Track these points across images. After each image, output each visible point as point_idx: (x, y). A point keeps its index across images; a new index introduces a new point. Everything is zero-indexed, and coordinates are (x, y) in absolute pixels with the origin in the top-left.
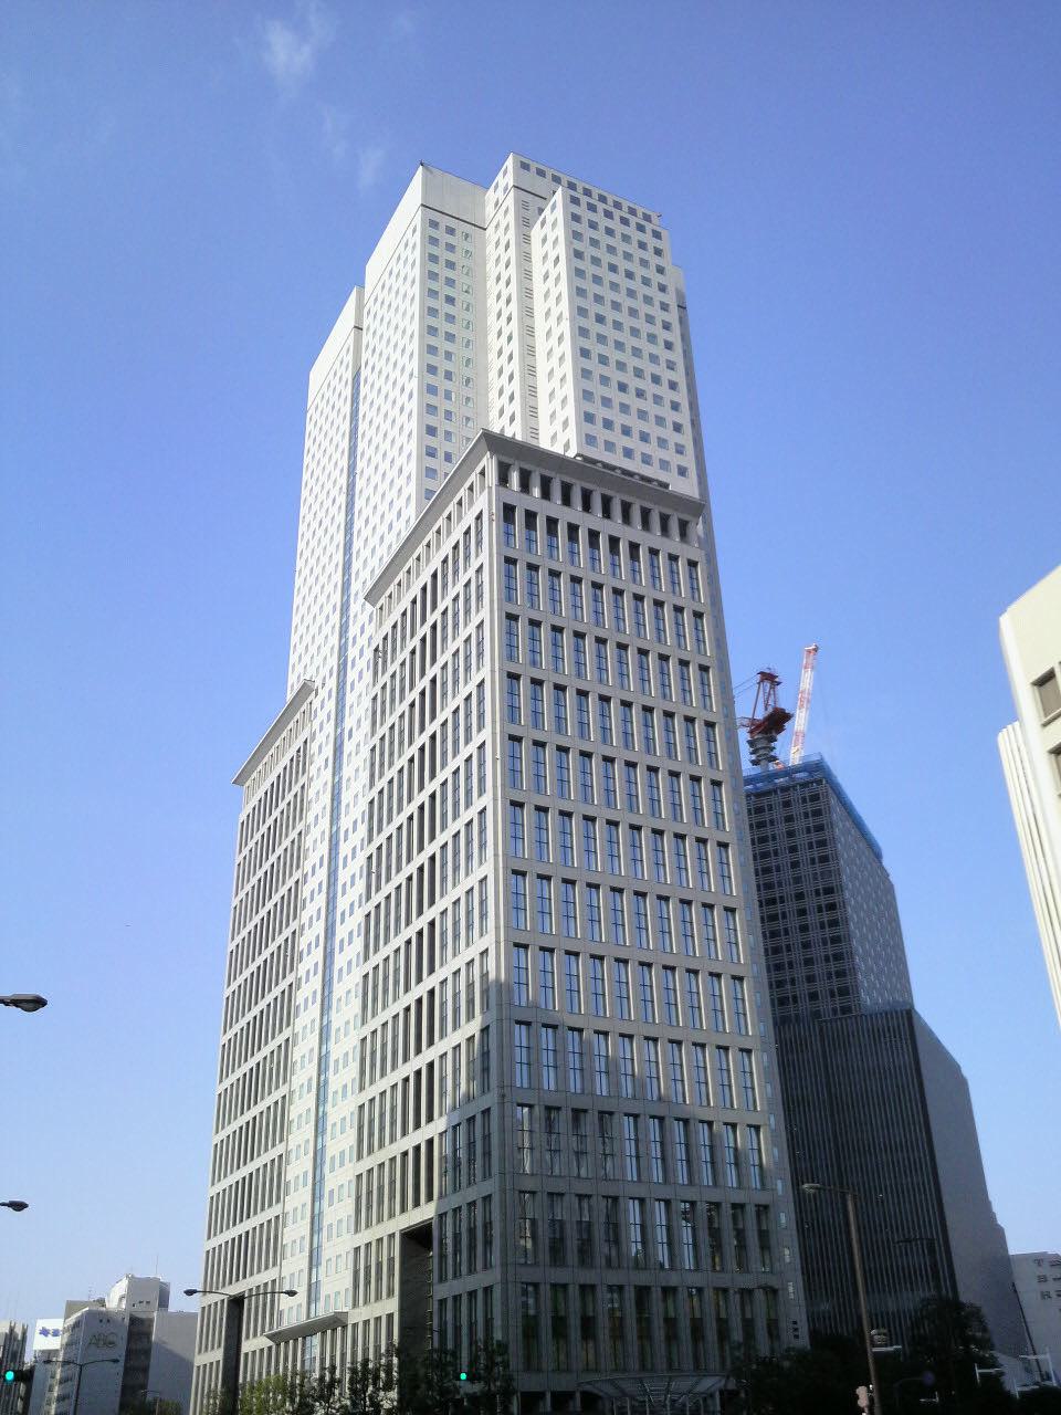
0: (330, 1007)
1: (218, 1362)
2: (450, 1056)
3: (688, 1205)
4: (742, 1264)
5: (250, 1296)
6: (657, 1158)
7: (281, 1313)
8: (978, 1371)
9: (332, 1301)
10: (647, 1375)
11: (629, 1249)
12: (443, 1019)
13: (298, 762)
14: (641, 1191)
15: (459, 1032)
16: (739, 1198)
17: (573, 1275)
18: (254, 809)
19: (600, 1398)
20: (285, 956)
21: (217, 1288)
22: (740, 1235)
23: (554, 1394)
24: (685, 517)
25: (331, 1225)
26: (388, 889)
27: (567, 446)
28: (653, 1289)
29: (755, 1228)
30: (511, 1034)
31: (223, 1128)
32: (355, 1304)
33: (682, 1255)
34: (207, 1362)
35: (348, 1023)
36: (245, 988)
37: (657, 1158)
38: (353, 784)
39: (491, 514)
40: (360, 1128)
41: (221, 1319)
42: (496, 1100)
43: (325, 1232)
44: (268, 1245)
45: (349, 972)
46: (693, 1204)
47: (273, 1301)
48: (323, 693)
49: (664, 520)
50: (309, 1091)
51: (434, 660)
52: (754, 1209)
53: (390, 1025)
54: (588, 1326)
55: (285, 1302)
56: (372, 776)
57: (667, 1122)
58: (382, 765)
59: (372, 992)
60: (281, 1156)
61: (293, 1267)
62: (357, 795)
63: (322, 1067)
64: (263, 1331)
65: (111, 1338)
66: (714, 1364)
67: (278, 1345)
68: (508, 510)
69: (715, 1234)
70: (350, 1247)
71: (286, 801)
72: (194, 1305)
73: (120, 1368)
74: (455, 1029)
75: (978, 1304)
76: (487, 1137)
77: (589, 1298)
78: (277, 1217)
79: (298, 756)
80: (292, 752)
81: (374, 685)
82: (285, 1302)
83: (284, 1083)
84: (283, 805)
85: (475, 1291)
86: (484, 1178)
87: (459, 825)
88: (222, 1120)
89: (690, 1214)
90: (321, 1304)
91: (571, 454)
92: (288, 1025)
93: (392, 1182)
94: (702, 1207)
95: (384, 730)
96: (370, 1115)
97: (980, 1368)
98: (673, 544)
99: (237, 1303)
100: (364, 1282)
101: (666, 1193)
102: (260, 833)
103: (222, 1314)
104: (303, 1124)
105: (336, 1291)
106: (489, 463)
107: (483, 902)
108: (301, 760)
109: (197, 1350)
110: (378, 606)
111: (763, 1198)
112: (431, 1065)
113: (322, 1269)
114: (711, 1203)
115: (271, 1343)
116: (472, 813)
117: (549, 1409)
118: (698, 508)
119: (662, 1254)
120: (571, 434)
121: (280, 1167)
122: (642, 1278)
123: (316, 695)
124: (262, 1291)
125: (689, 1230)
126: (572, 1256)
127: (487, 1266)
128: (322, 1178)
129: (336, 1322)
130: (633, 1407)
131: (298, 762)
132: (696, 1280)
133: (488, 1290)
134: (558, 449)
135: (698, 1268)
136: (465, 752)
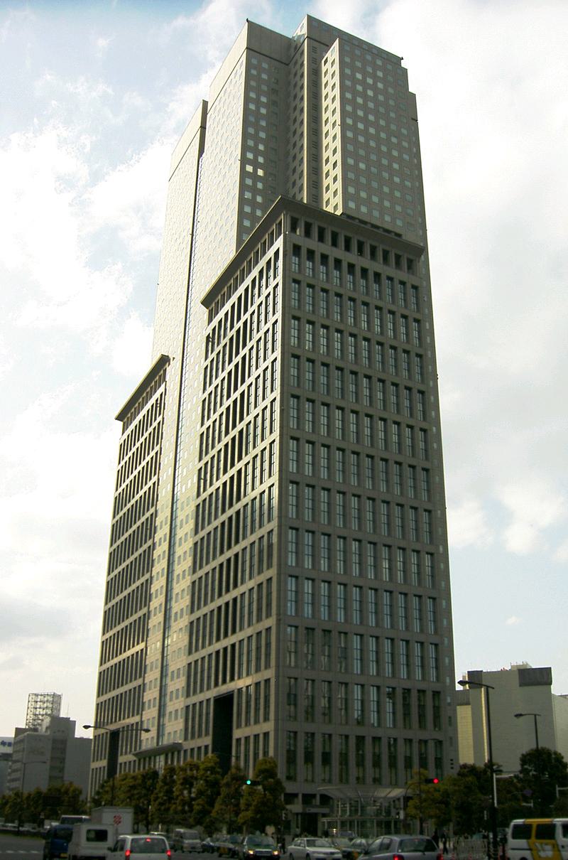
0: (171, 599)
1: (104, 767)
2: (247, 595)
3: (391, 689)
4: (422, 724)
5: (123, 731)
6: (371, 566)
7: (141, 741)
8: (558, 789)
9: (172, 736)
11: (353, 714)
12: (245, 527)
14: (362, 680)
16: (422, 686)
17: (319, 727)
18: (125, 441)
19: (332, 798)
21: (104, 725)
22: (422, 707)
25: (173, 672)
26: (213, 452)
27: (336, 207)
28: (367, 738)
30: (288, 443)
31: (110, 601)
32: (186, 739)
33: (385, 719)
35: (186, 534)
36: (119, 578)
37: (371, 566)
38: (182, 582)
40: (189, 677)
42: (275, 623)
43: (168, 697)
44: (134, 702)
45: (184, 577)
46: (394, 689)
47: (136, 735)
49: (398, 258)
50: (162, 576)
52: (431, 693)
53: (210, 575)
54: (326, 759)
55: (144, 735)
57: (381, 639)
60: (142, 650)
61: (150, 714)
63: (168, 599)
64: (131, 751)
67: (140, 760)
68: (297, 250)
69: (407, 706)
70: (185, 663)
72: (89, 734)
73: (47, 766)
75: (563, 754)
78: (140, 686)
79: (157, 404)
80: (153, 401)
81: (204, 392)
82: (144, 735)
83: (150, 538)
84: (146, 435)
86: (266, 668)
89: (391, 695)
90: (166, 738)
91: (339, 213)
94: (399, 693)
95: (212, 388)
97: (559, 787)
99: (115, 735)
101: (378, 682)
102: (132, 452)
103: (104, 774)
104: (158, 613)
105: (174, 729)
108: (159, 405)
109: (92, 759)
110: (210, 308)
111: (437, 687)
113: (169, 678)
114: (404, 689)
115: (135, 758)
116: (266, 443)
119: (373, 718)
120: (339, 199)
121: (139, 693)
122: (361, 731)
124: (130, 728)
125: (391, 704)
126: (318, 716)
128: (165, 705)
129: (173, 750)
132: (394, 733)
134: (330, 209)
136: (263, 366)
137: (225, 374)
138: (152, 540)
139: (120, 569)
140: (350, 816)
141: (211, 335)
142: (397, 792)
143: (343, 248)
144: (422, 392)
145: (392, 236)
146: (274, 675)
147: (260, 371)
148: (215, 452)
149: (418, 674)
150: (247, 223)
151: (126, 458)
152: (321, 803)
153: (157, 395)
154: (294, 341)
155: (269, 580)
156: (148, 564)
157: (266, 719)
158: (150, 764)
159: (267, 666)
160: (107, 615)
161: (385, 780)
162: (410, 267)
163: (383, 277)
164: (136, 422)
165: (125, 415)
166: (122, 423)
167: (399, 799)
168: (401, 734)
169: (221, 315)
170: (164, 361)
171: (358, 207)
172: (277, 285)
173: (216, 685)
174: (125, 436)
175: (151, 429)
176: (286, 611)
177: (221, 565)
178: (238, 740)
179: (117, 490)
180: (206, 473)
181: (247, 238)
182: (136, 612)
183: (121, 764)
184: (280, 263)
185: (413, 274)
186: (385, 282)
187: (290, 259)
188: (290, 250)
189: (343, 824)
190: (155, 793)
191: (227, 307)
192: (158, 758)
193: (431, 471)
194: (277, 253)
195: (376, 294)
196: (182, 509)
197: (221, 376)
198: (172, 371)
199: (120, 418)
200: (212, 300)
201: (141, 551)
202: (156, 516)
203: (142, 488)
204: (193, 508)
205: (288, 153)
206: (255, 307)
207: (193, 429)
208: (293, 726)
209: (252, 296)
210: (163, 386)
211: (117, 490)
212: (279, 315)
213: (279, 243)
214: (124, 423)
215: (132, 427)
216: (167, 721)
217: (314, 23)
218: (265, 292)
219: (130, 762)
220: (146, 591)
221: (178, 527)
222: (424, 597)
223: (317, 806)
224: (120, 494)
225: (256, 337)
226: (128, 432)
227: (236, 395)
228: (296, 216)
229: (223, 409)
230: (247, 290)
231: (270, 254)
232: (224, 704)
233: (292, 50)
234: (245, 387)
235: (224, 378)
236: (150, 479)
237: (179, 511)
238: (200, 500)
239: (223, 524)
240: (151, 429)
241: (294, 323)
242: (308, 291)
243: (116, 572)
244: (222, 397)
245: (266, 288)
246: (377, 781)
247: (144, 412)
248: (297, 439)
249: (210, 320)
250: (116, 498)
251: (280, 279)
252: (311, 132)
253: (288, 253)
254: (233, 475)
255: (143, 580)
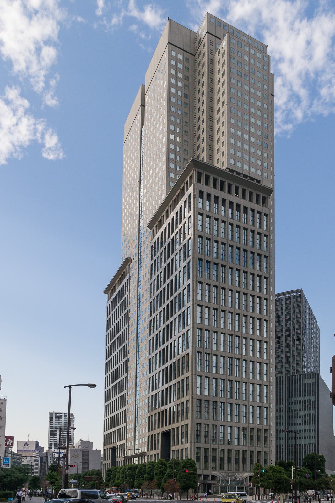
1: (109, 463)
10: (230, 472)
13: (125, 287)
15: (179, 378)
18: (109, 305)
20: (124, 352)
23: (203, 475)
24: (265, 196)
27: (223, 164)
29: (263, 435)
30: (196, 308)
32: (148, 451)
34: (106, 463)
39: (194, 195)
41: (110, 452)
44: (123, 433)
48: (133, 262)
51: (172, 252)
56: (152, 256)
58: (155, 270)
59: (152, 345)
60: (125, 410)
62: (145, 305)
65: (78, 456)
66: (248, 469)
68: (201, 193)
71: (122, 300)
74: (178, 377)
76: (187, 408)
77: (215, 452)
78: (125, 427)
79: (125, 285)
80: (123, 283)
85: (183, 449)
87: (181, 312)
88: (106, 400)
92: (126, 340)
93: (159, 419)
95: (155, 258)
96: (152, 420)
98: (259, 208)
99: (114, 450)
100: (150, 445)
106: (194, 173)
107: (188, 362)
108: (127, 285)
110: (153, 230)
111: (266, 428)
112: (170, 387)
116: (185, 285)
117: (202, 479)
118: (270, 191)
122: (230, 447)
123: (131, 263)
127: (187, 418)
129: (143, 455)
130: (225, 479)
131: (125, 287)
132: (245, 449)
133: (187, 425)
134: (219, 165)
135: (246, 445)
136: (183, 287)
137: (162, 269)
138: (127, 357)
139: (111, 371)
140: (225, 484)
141: (153, 246)
142: (247, 475)
143: (227, 192)
144: (266, 278)
145: (255, 182)
146: (190, 446)
147: (181, 268)
148: (158, 293)
149: (258, 422)
150: (172, 175)
151: (111, 314)
152: (211, 479)
153: (125, 280)
154: (199, 297)
155: (187, 378)
156: (126, 369)
157: (187, 418)
158: (131, 462)
159: (187, 394)
160: (106, 379)
161: (241, 469)
162: (264, 202)
163: (249, 209)
164: (115, 295)
165: (108, 291)
166: (107, 295)
167: (247, 477)
168: (248, 449)
169: (159, 234)
170: (128, 261)
171: (236, 163)
172: (190, 216)
173: (162, 426)
174: (110, 302)
175: (123, 299)
176: (196, 392)
177: (163, 370)
178: (173, 451)
179: (107, 317)
180: (154, 324)
181: (172, 185)
182: (121, 376)
183: (117, 462)
184: (192, 202)
185: (265, 207)
186: (250, 213)
187: (198, 200)
188: (197, 195)
189: (222, 488)
190: (134, 477)
191: (162, 229)
192: (135, 459)
193: (269, 257)
194: (190, 196)
195: (244, 220)
196: (143, 279)
197: (160, 251)
198: (133, 267)
199: (106, 292)
200: (154, 225)
201: (122, 362)
202: (129, 329)
203: (118, 317)
204: (149, 304)
205: (195, 125)
206: (178, 230)
207: (145, 319)
208: (198, 445)
209: (176, 223)
210: (128, 275)
211: (107, 317)
212: (191, 281)
213: (191, 190)
214: (108, 295)
215: (113, 297)
216: (138, 442)
217: (212, 20)
218: (183, 221)
219: (122, 461)
220: (126, 382)
221: (141, 315)
222: (262, 363)
223: (210, 481)
224: (109, 319)
225: (179, 269)
226: (111, 300)
227: (168, 281)
228: (201, 171)
229: (162, 289)
230: (173, 219)
231: (186, 197)
232: (166, 435)
233: (197, 42)
234: (173, 256)
235: (162, 271)
236: (125, 326)
237: (140, 342)
238: (151, 337)
239: (163, 349)
240: (123, 299)
241: (200, 217)
242: (207, 220)
243: (110, 343)
244: (161, 282)
245: (184, 218)
246: (237, 470)
247: (119, 289)
248: (201, 306)
249: (153, 237)
250: (106, 363)
251: (191, 213)
252: (210, 62)
253: (196, 196)
254: (167, 300)
255: (124, 360)
